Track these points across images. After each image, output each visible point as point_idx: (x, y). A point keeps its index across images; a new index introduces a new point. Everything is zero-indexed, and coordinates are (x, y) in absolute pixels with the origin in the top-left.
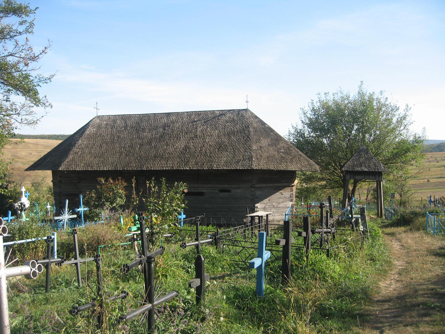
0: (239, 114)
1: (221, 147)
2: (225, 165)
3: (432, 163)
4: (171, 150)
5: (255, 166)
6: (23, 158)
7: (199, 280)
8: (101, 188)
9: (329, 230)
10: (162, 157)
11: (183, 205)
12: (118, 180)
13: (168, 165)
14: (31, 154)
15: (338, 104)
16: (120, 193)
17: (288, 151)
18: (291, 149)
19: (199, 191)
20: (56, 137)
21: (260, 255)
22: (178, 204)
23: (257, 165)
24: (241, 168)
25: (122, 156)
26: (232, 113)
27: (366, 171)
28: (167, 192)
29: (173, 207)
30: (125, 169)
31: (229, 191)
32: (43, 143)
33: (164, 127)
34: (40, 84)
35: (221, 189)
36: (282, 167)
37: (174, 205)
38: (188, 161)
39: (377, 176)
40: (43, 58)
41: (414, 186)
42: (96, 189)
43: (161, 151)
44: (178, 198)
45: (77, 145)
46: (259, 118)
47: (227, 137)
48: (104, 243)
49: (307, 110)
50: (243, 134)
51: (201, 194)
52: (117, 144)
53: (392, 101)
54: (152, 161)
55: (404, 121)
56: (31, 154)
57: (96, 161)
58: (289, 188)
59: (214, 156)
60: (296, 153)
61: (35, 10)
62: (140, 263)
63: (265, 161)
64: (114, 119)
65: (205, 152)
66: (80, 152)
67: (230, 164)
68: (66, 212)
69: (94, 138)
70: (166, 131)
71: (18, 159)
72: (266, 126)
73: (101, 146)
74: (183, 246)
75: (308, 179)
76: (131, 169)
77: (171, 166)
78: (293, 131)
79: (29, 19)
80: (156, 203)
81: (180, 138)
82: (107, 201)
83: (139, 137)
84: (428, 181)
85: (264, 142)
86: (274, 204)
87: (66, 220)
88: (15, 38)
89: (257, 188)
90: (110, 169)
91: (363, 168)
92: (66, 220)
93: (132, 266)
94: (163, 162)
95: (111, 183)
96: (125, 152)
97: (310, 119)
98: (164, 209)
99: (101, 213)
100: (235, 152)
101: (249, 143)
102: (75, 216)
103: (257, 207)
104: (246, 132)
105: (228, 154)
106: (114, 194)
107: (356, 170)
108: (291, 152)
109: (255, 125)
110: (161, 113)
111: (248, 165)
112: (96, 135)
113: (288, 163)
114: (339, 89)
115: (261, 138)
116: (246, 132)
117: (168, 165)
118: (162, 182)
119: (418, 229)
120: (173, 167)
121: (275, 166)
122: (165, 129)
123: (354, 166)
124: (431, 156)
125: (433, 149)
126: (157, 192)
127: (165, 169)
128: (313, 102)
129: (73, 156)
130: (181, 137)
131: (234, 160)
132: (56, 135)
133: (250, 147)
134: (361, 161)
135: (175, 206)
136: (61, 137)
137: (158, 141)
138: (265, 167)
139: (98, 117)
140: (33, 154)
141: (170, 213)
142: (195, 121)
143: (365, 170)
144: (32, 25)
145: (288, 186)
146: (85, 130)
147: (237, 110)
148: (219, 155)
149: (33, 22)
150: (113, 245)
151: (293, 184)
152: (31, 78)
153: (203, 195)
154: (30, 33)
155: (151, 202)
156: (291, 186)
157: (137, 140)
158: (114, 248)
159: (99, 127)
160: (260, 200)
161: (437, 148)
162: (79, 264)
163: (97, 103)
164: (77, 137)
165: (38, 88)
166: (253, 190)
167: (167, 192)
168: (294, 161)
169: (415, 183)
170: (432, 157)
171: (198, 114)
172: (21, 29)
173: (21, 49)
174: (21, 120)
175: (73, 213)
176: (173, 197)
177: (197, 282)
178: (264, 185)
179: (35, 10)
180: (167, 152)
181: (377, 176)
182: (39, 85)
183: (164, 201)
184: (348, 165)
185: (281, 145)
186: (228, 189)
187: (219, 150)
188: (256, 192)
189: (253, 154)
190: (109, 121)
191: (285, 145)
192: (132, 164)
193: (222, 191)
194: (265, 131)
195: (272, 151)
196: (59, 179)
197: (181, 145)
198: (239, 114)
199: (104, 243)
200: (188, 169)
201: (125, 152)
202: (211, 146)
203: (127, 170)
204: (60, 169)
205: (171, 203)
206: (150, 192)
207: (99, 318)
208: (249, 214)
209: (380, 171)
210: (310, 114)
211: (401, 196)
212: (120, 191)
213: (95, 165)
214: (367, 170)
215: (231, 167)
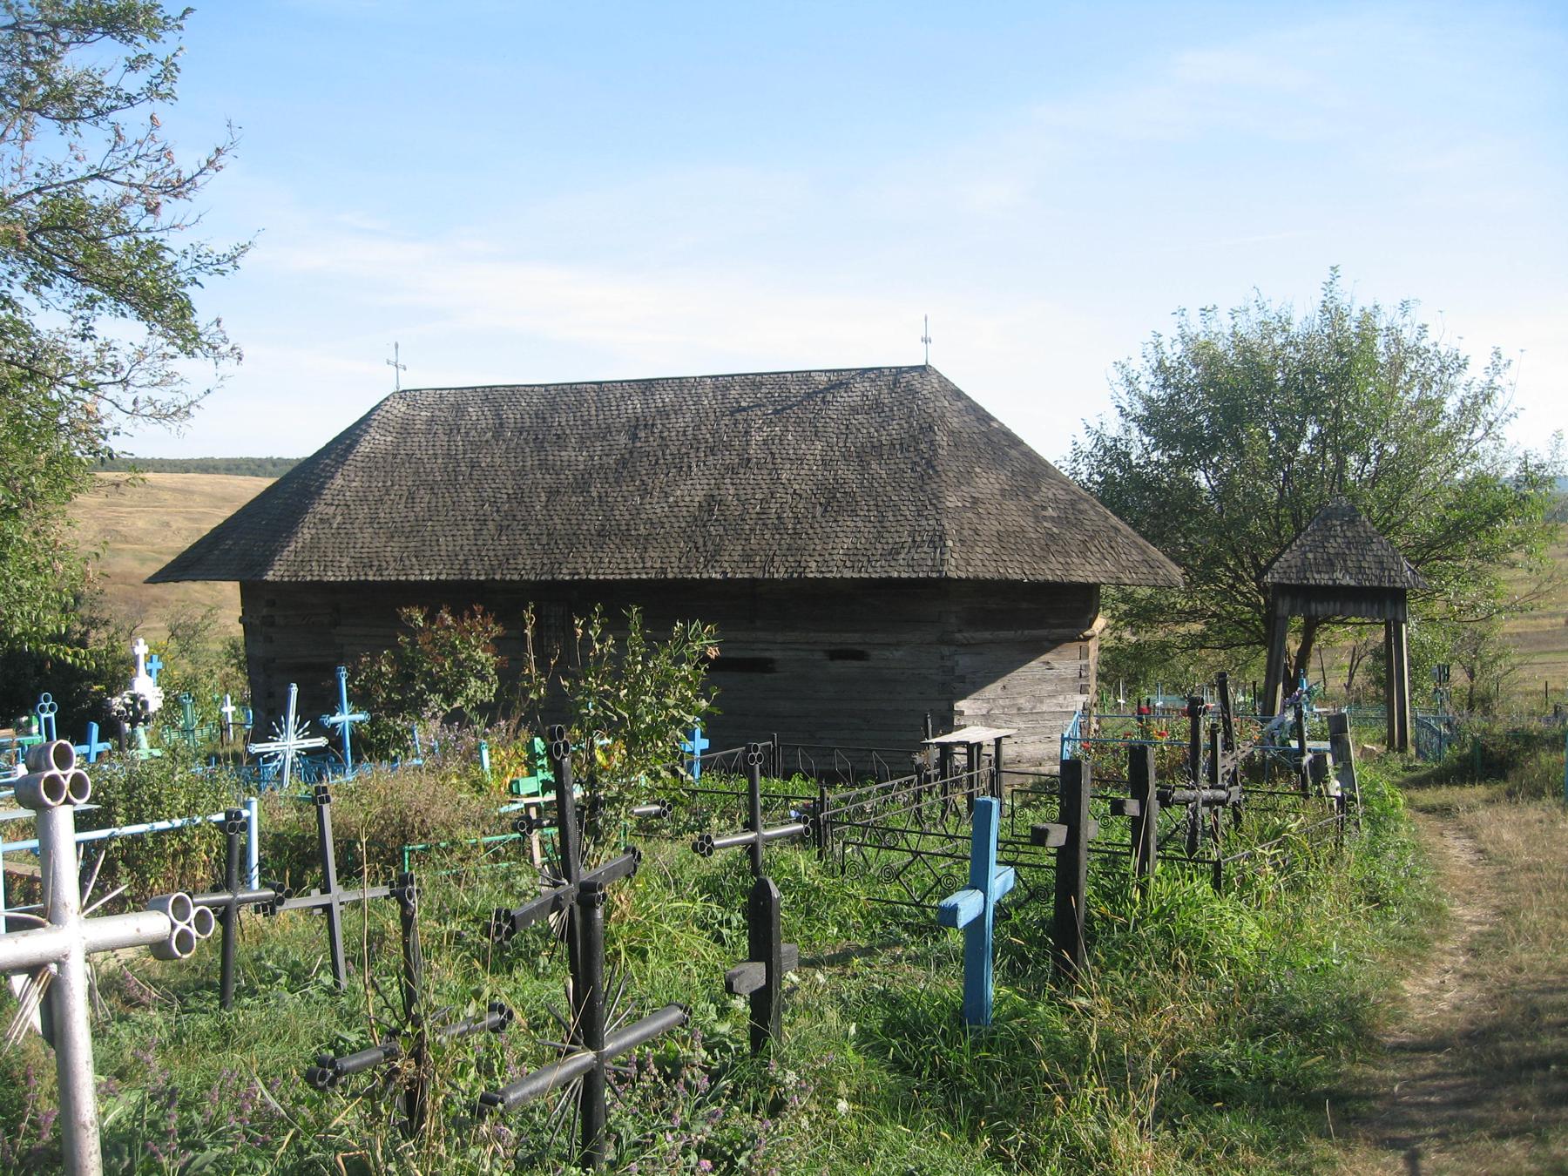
1: (832, 500)
5: (955, 568)
6: (138, 541)
7: (761, 966)
8: (413, 644)
9: (1222, 794)
11: (704, 703)
12: (473, 616)
13: (649, 564)
14: (168, 524)
16: (478, 662)
18: (1081, 507)
19: (757, 654)
20: (253, 467)
21: (979, 881)
22: (684, 699)
23: (962, 562)
24: (904, 575)
25: (485, 532)
27: (1348, 587)
28: (646, 658)
29: (667, 708)
30: (498, 577)
31: (860, 656)
32: (208, 489)
33: (634, 428)
34: (201, 277)
35: (832, 648)
36: (1051, 571)
37: (670, 702)
38: (719, 550)
39: (1388, 603)
40: (211, 189)
42: (395, 647)
43: (621, 514)
44: (684, 679)
45: (327, 495)
46: (968, 398)
47: (854, 465)
48: (425, 836)
50: (912, 455)
51: (763, 666)
52: (466, 489)
53: (1442, 337)
54: (590, 548)
56: (168, 524)
58: (1076, 645)
59: (810, 531)
61: (182, 17)
62: (556, 905)
63: (989, 551)
64: (457, 402)
66: (339, 518)
68: (292, 727)
70: (639, 444)
71: (121, 542)
72: (995, 425)
73: (411, 497)
74: (704, 847)
76: (516, 577)
77: (658, 565)
78: (1087, 444)
80: (607, 695)
81: (690, 467)
83: (543, 466)
85: (988, 483)
86: (1022, 701)
87: (289, 757)
88: (113, 116)
89: (962, 645)
90: (443, 577)
92: (289, 757)
94: (631, 553)
95: (448, 628)
96: (497, 518)
98: (636, 718)
100: (882, 518)
101: (934, 486)
102: (321, 742)
103: (961, 713)
104: (922, 446)
105: (860, 524)
108: (1081, 517)
109: (955, 423)
110: (622, 382)
111: (930, 563)
112: (395, 456)
113: (1070, 556)
114: (1254, 296)
115: (977, 470)
116: (922, 446)
117: (649, 564)
118: (628, 620)
121: (1025, 565)
122: (634, 437)
123: (1304, 568)
126: (611, 656)
127: (635, 576)
128: (1161, 340)
129: (313, 531)
130: (694, 464)
131: (879, 546)
132: (253, 460)
133: (936, 499)
134: (1331, 551)
135: (675, 707)
136: (270, 467)
138: (989, 572)
139: (402, 394)
140: (174, 526)
141: (657, 731)
142: (741, 410)
143: (1344, 582)
144: (170, 69)
145: (1072, 640)
146: (357, 442)
147: (890, 368)
148: (828, 530)
150: (453, 843)
151: (1088, 633)
153: (772, 671)
154: (162, 97)
156: (1080, 640)
157: (539, 476)
158: (458, 854)
159: (405, 429)
160: (970, 685)
162: (336, 909)
164: (327, 465)
166: (946, 650)
167: (646, 658)
168: (1094, 549)
169: (1520, 630)
171: (753, 383)
172: (134, 83)
174: (135, 402)
176: (670, 676)
177: (755, 974)
178: (987, 635)
179: (182, 17)
181: (1388, 603)
182: (195, 281)
183: (636, 689)
184: (1286, 565)
185: (1047, 492)
187: (826, 511)
188: (957, 658)
189: (947, 527)
190: (440, 410)
191: (1061, 494)
193: (837, 655)
194: (990, 442)
195: (1015, 515)
196: (265, 612)
197: (692, 491)
199: (425, 836)
200: (718, 576)
201: (497, 518)
202: (800, 496)
203: (502, 581)
204: (270, 576)
205: (659, 695)
206: (585, 657)
207: (410, 1098)
208: (934, 737)
209: (1398, 585)
210: (1148, 384)
212: (480, 655)
213: (393, 564)
214: (1353, 583)
215: (870, 570)
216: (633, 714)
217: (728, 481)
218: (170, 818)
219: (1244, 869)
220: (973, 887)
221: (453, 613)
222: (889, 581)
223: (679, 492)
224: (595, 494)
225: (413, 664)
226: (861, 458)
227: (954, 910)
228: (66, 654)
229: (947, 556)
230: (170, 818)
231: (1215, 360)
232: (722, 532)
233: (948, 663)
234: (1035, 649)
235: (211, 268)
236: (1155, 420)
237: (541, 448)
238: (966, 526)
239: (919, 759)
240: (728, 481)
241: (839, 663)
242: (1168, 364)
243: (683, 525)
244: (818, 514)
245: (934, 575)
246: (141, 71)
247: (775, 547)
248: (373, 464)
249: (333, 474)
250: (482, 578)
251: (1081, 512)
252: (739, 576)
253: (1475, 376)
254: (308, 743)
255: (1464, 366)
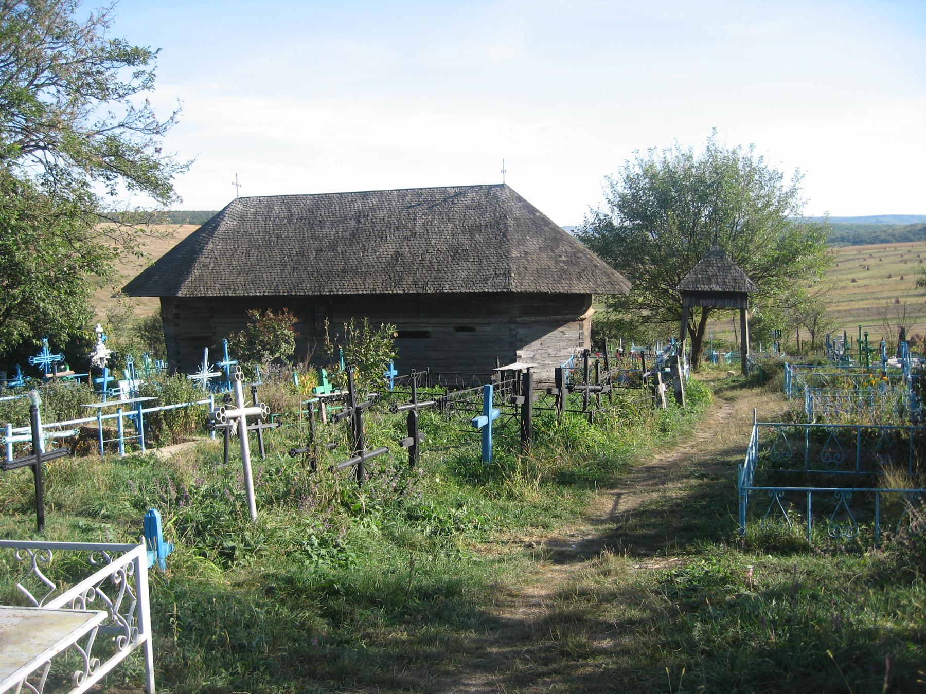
0: (489, 193)
1: (457, 254)
2: (464, 285)
3: (909, 265)
4: (371, 259)
5: (515, 288)
7: (412, 439)
8: (255, 327)
9: (599, 387)
10: (355, 272)
11: (393, 354)
12: (283, 313)
13: (367, 287)
15: (670, 170)
16: (286, 335)
17: (574, 258)
19: (421, 329)
21: (486, 413)
22: (385, 352)
23: (519, 284)
24: (490, 291)
25: (286, 271)
26: (477, 192)
27: (718, 292)
28: (371, 337)
29: (379, 356)
30: (293, 294)
31: (471, 329)
33: (358, 217)
34: (174, 174)
36: (562, 288)
37: (380, 353)
38: (401, 279)
39: (739, 301)
40: (172, 131)
41: (844, 313)
42: (246, 328)
43: (353, 261)
44: (385, 344)
45: (205, 252)
46: (525, 201)
47: (467, 236)
48: (280, 410)
49: (617, 179)
50: (496, 230)
51: (424, 335)
52: (275, 249)
53: (770, 165)
54: (338, 279)
55: (790, 200)
57: (241, 279)
58: (577, 323)
59: (446, 269)
60: (588, 263)
61: (157, 53)
62: (349, 414)
63: (532, 278)
64: (268, 204)
65: (430, 263)
66: (212, 265)
67: (472, 283)
68: (206, 367)
69: (235, 239)
70: (361, 226)
72: (537, 214)
73: (248, 253)
74: (394, 410)
75: (621, 305)
76: (302, 294)
77: (372, 287)
79: (148, 69)
80: (357, 351)
81: (386, 237)
82: (265, 349)
83: (313, 237)
84: (897, 302)
85: (533, 244)
86: (550, 351)
87: (205, 381)
88: (127, 97)
89: (520, 324)
90: (266, 294)
91: (713, 286)
92: (205, 381)
93: (341, 416)
94: (359, 281)
95: (271, 319)
96: (292, 264)
97: (623, 197)
98: (367, 360)
99: (255, 369)
100: (480, 263)
102: (219, 374)
104: (501, 226)
105: (470, 265)
106: (276, 336)
107: (700, 289)
108: (578, 260)
109: (517, 213)
110: (351, 193)
111: (503, 285)
112: (238, 232)
113: (572, 280)
114: (674, 143)
115: (528, 237)
116: (501, 226)
117: (367, 287)
118: (363, 323)
119: (774, 391)
120: (374, 289)
122: (359, 222)
123: (697, 282)
124: (909, 248)
125: (914, 235)
126: (358, 337)
127: (361, 292)
128: (629, 164)
129: (200, 271)
130: (388, 236)
131: (479, 276)
134: (710, 274)
135: (382, 355)
137: (348, 244)
138: (532, 289)
139: (240, 200)
141: (376, 365)
142: (411, 207)
143: (716, 290)
144: (152, 77)
146: (219, 225)
149: (154, 72)
150: (290, 413)
151: (582, 317)
152: (161, 167)
153: (428, 337)
154: (149, 88)
155: (350, 351)
156: (579, 320)
157: (311, 242)
158: (292, 418)
159: (243, 218)
160: (524, 342)
161: (923, 233)
162: (261, 431)
163: (236, 175)
164: (204, 237)
165: (171, 181)
166: (512, 326)
167: (371, 337)
168: (584, 276)
169: (869, 306)
170: (909, 251)
171: (418, 193)
172: (136, 83)
173: (137, 117)
174: (151, 232)
175: (216, 369)
176: (380, 344)
177: (410, 441)
178: (533, 319)
179: (157, 53)
180: (364, 262)
181: (739, 301)
182: (171, 176)
183: (367, 349)
184: (687, 281)
185: (562, 248)
186: (470, 326)
187: (453, 259)
190: (260, 208)
191: (569, 249)
192: (304, 285)
193: (460, 329)
194: (534, 223)
195: (545, 260)
196: (174, 311)
197: (387, 250)
198: (489, 193)
199: (280, 410)
200: (401, 292)
201: (292, 264)
202: (441, 252)
203: (296, 295)
204: (180, 294)
205: (376, 351)
206: (348, 338)
207: (313, 463)
208: (501, 366)
209: (743, 291)
210: (622, 188)
211: (813, 334)
212: (286, 332)
213: (241, 288)
214: (720, 290)
216: (366, 358)
217: (405, 244)
218: (181, 403)
219: (603, 416)
220: (484, 415)
221: (272, 312)
222: (484, 293)
223: (381, 250)
224: (339, 251)
225: (256, 337)
226: (472, 231)
227: (477, 422)
228: (85, 334)
229: (511, 281)
230: (181, 403)
231: (654, 176)
232: (403, 270)
233: (514, 333)
234: (556, 325)
235: (178, 170)
236: (626, 205)
237: (312, 228)
238: (521, 266)
239: (493, 378)
240: (405, 244)
241: (461, 333)
242: (632, 176)
243: (384, 266)
244: (449, 261)
245: (505, 291)
246: (140, 78)
247: (428, 277)
248: (227, 235)
249: (208, 241)
250: (286, 294)
251: (578, 258)
252: (411, 292)
253: (786, 185)
254: (214, 375)
255: (781, 177)
